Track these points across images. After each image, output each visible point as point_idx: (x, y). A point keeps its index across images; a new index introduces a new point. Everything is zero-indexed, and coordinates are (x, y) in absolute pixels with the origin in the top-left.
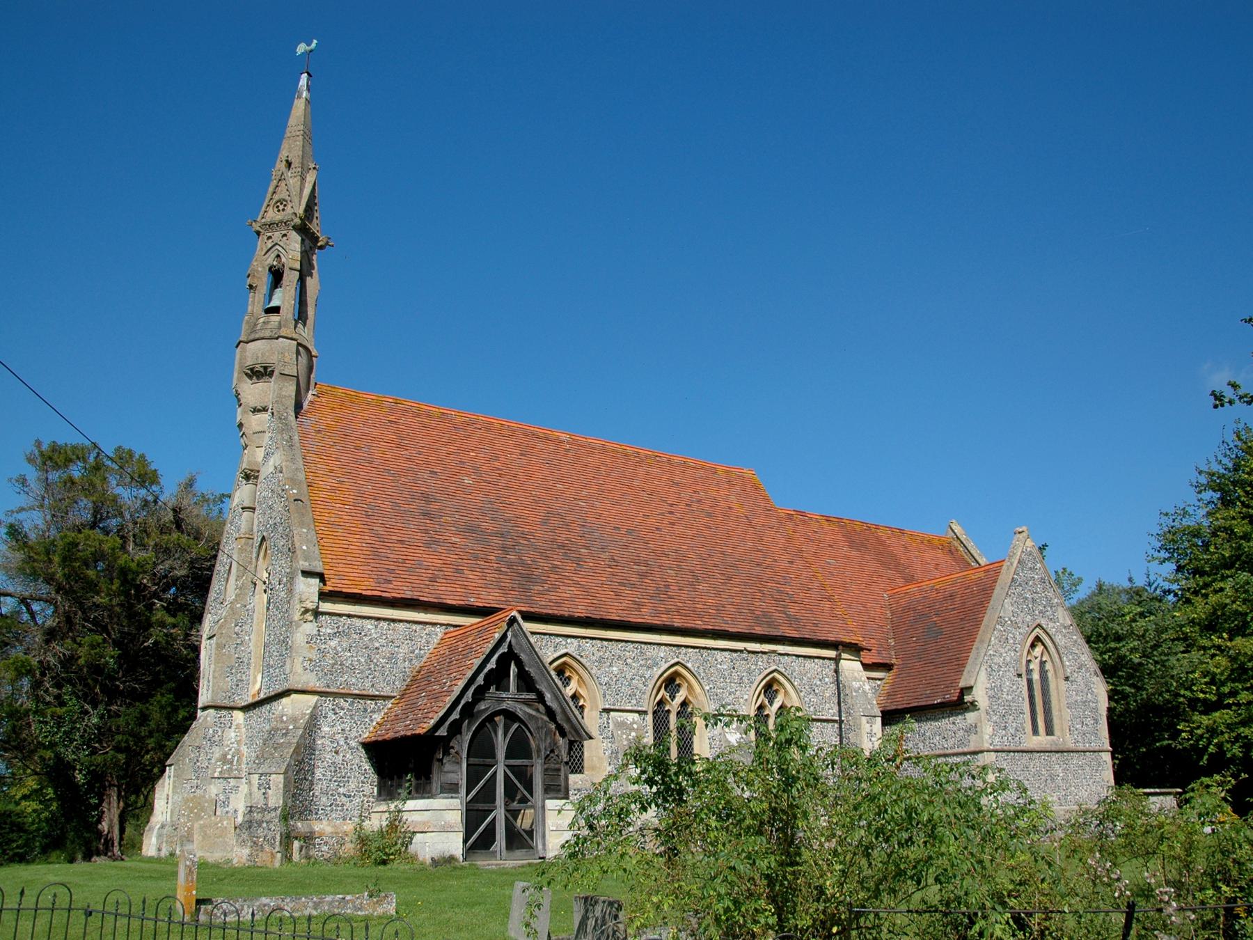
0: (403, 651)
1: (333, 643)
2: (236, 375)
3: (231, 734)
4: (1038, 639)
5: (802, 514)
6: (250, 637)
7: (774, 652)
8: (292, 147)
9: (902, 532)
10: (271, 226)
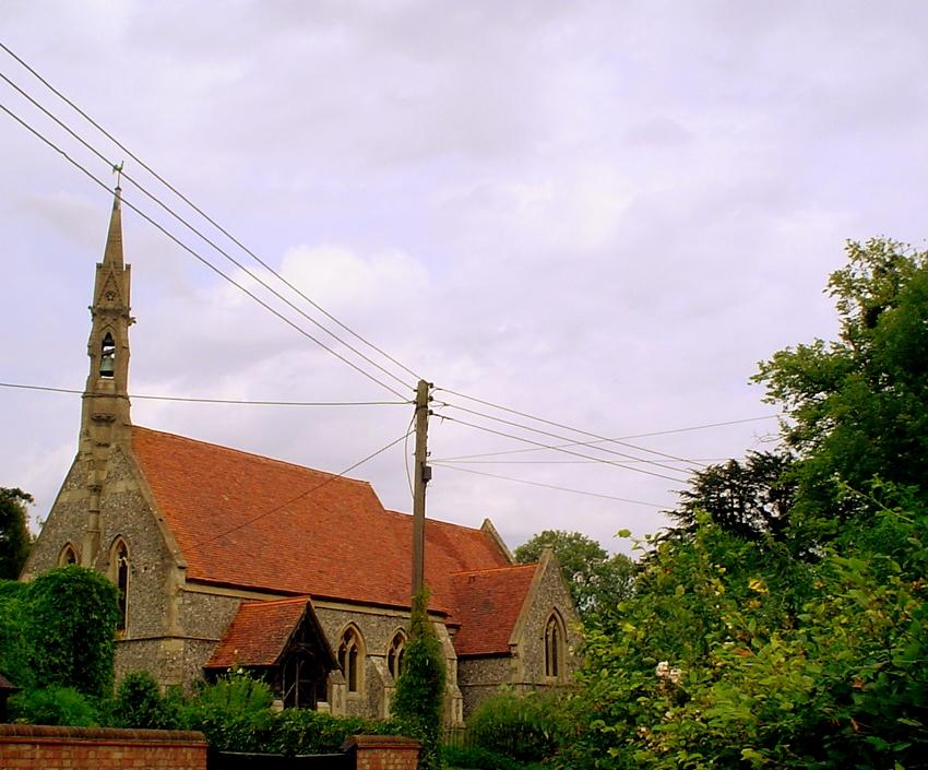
4: (553, 617)
7: (400, 617)
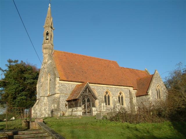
0: (70, 88)
1: (61, 87)
2: (42, 49)
3: (45, 100)
5: (123, 68)
6: (43, 88)
8: (49, 14)
9: (138, 70)
10: (46, 27)
